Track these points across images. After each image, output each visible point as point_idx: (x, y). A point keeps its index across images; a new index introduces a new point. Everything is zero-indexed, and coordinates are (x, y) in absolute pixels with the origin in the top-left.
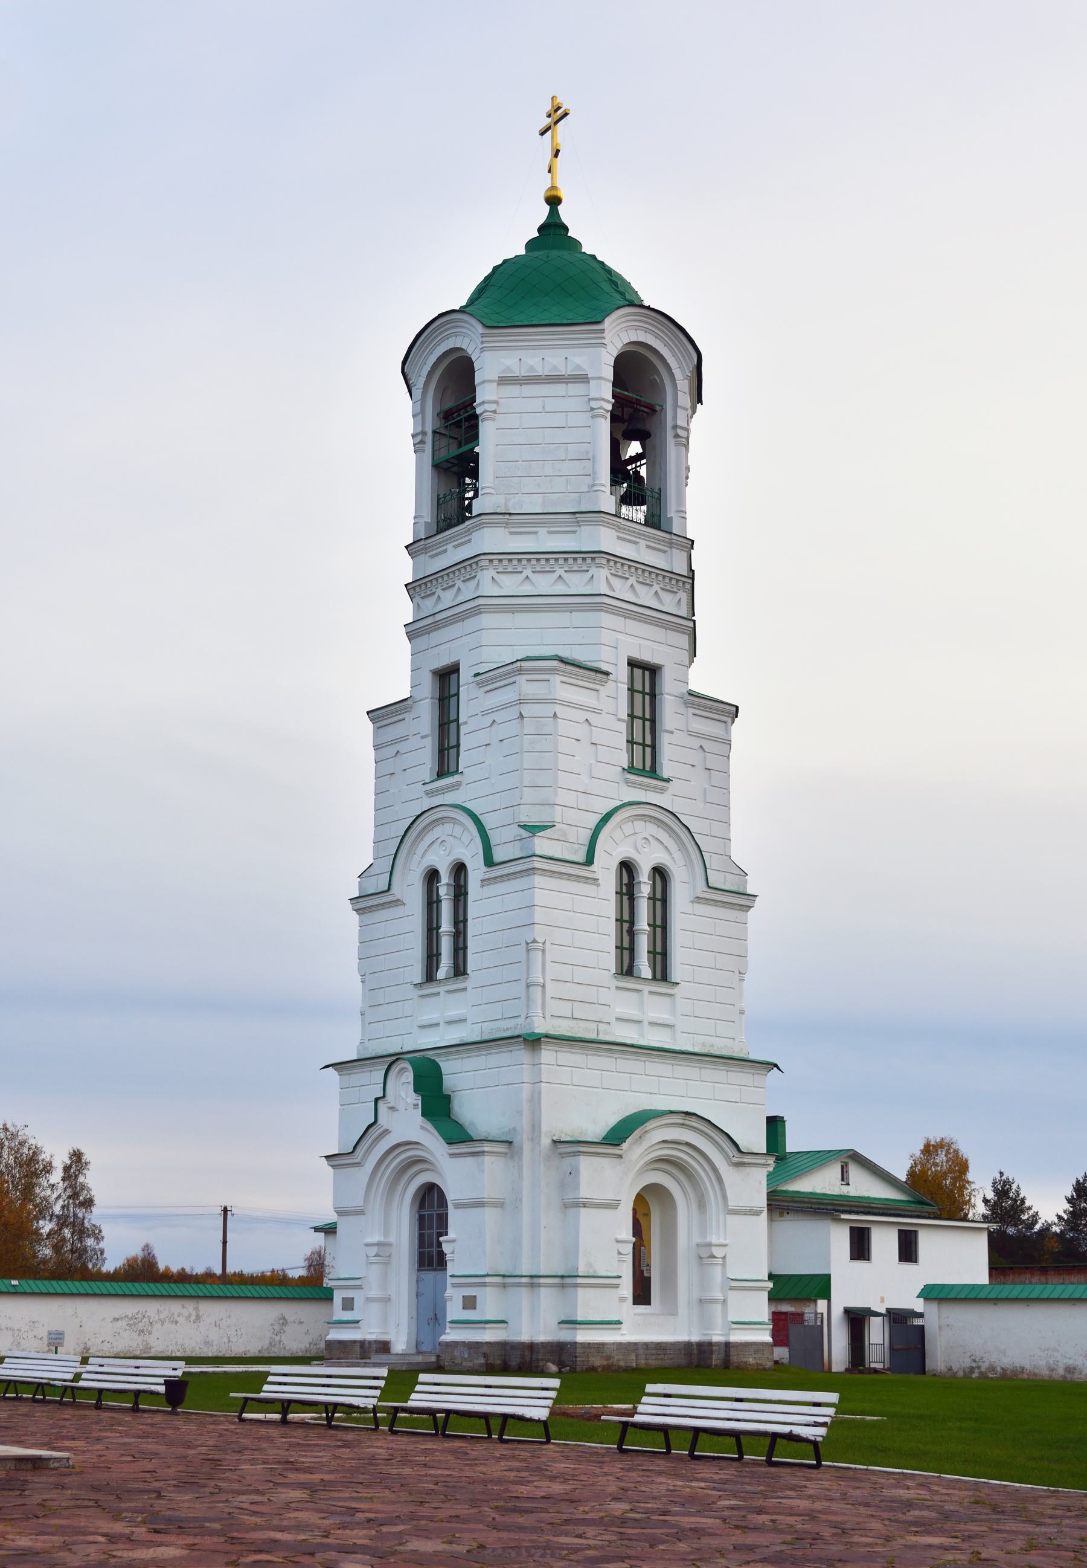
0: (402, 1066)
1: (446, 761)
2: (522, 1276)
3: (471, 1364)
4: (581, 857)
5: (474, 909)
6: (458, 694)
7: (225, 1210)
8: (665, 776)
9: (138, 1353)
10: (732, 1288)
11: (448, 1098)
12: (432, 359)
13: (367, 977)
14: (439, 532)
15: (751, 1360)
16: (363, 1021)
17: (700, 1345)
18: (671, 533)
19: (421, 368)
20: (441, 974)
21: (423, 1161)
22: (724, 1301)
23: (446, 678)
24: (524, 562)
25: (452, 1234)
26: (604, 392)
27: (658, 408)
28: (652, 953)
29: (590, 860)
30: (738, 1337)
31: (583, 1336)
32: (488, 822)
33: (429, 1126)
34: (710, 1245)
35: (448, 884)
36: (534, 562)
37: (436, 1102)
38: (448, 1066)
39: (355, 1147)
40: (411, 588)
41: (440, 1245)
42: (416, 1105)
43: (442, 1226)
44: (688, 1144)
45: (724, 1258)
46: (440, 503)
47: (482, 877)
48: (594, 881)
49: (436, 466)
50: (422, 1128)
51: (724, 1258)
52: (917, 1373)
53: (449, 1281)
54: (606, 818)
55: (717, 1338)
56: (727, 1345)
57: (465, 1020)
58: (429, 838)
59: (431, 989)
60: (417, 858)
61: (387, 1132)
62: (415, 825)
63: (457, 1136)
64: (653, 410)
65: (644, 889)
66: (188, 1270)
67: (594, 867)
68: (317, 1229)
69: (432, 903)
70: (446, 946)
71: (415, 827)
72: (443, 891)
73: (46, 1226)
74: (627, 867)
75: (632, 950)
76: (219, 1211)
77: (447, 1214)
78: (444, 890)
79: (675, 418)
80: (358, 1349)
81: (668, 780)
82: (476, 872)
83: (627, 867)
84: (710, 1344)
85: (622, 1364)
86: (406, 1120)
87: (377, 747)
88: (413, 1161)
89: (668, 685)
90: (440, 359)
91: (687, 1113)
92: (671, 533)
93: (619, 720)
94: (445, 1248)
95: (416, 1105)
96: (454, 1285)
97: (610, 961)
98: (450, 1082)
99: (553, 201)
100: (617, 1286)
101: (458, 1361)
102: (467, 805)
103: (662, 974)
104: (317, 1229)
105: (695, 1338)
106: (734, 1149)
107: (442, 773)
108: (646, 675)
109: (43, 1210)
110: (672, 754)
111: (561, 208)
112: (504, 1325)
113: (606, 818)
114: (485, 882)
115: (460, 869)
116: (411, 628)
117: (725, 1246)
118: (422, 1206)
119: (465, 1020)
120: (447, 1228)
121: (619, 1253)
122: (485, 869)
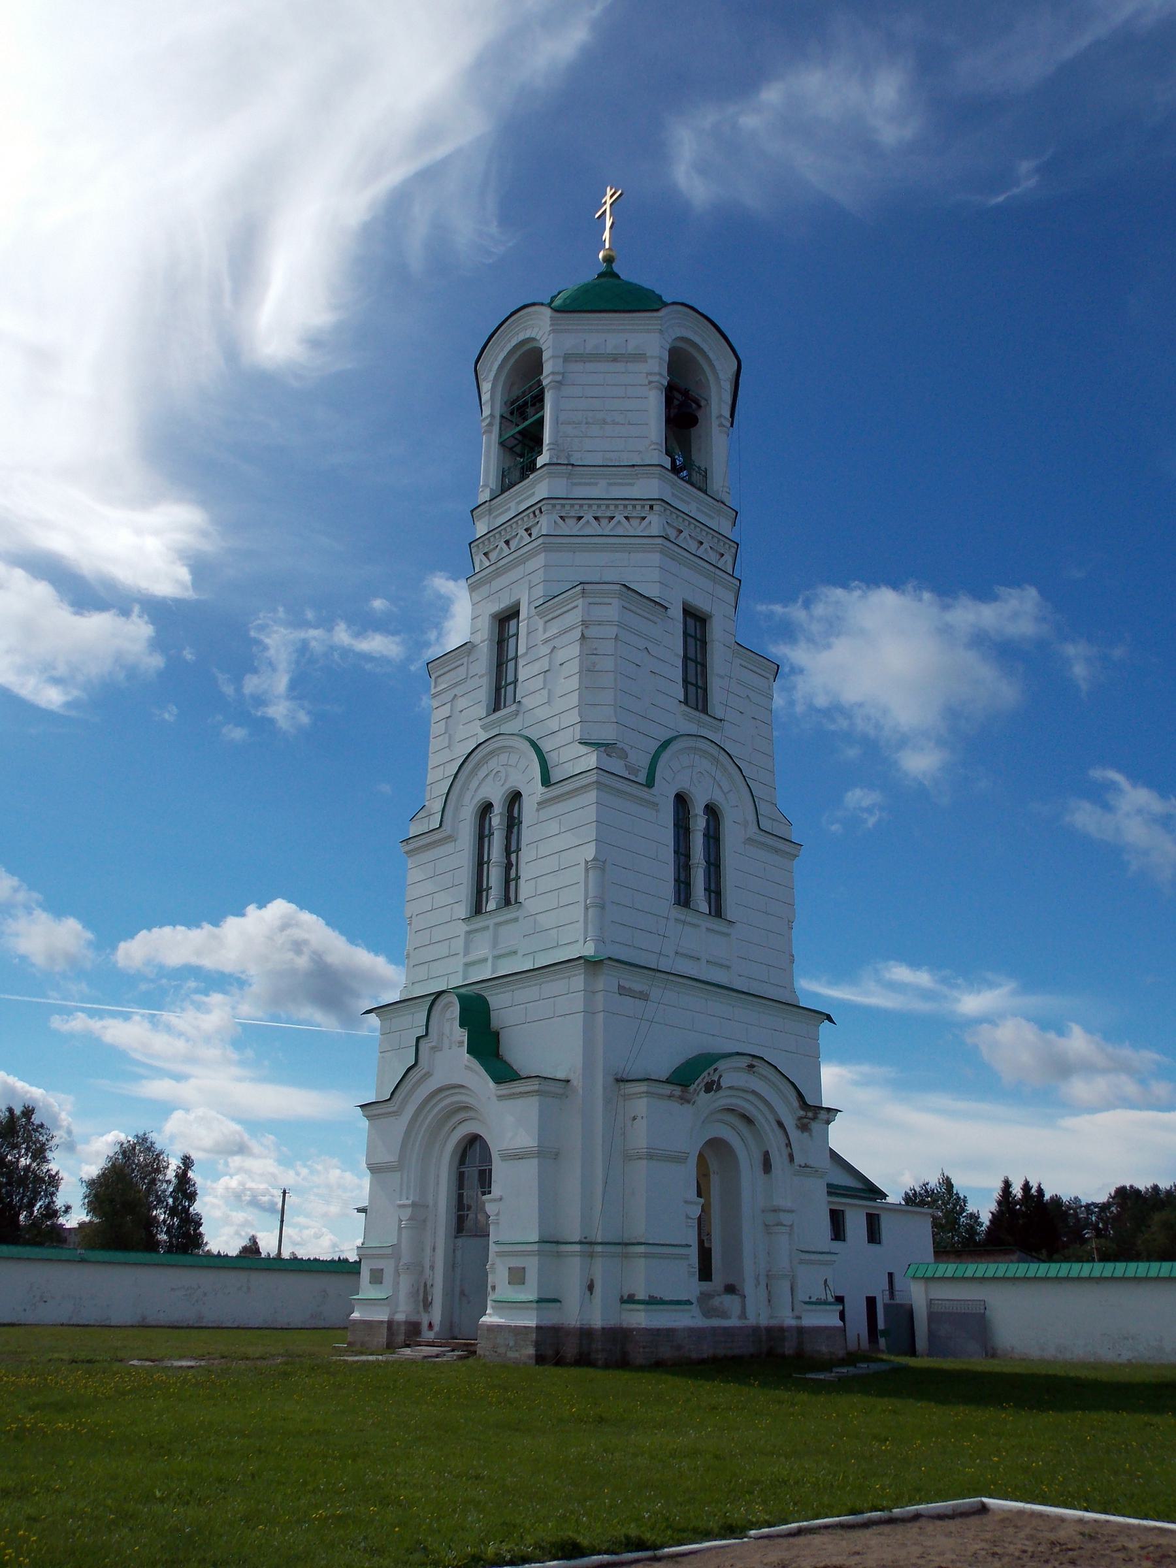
3: (516, 1355)
4: (642, 778)
8: (719, 715)
9: (191, 1323)
10: (802, 1262)
11: (497, 1035)
14: (503, 491)
15: (824, 1349)
17: (769, 1330)
19: (492, 364)
21: (467, 1108)
23: (506, 619)
24: (585, 508)
27: (703, 403)
28: (707, 889)
29: (650, 783)
31: (639, 1319)
34: (775, 1210)
37: (485, 1043)
38: (496, 1000)
39: (392, 1094)
43: (485, 1180)
44: (753, 1092)
47: (539, 800)
49: (502, 444)
50: (467, 1067)
51: (791, 1226)
52: (905, 1354)
53: (493, 1248)
54: (665, 745)
55: (790, 1322)
56: (801, 1330)
57: (515, 953)
59: (480, 922)
60: (469, 794)
61: (428, 1075)
63: (502, 1072)
65: (699, 823)
67: (654, 791)
69: (482, 836)
73: (160, 1214)
74: (681, 801)
75: (688, 884)
77: (490, 1170)
78: (497, 820)
82: (533, 792)
83: (681, 801)
84: (782, 1329)
85: (694, 1355)
86: (454, 1061)
89: (717, 632)
90: (511, 353)
91: (754, 1056)
93: (677, 655)
96: (500, 1254)
98: (497, 1020)
101: (502, 1350)
102: (525, 732)
103: (717, 910)
109: (160, 1201)
113: (665, 745)
114: (542, 804)
115: (515, 797)
118: (462, 1161)
119: (515, 953)
122: (543, 790)
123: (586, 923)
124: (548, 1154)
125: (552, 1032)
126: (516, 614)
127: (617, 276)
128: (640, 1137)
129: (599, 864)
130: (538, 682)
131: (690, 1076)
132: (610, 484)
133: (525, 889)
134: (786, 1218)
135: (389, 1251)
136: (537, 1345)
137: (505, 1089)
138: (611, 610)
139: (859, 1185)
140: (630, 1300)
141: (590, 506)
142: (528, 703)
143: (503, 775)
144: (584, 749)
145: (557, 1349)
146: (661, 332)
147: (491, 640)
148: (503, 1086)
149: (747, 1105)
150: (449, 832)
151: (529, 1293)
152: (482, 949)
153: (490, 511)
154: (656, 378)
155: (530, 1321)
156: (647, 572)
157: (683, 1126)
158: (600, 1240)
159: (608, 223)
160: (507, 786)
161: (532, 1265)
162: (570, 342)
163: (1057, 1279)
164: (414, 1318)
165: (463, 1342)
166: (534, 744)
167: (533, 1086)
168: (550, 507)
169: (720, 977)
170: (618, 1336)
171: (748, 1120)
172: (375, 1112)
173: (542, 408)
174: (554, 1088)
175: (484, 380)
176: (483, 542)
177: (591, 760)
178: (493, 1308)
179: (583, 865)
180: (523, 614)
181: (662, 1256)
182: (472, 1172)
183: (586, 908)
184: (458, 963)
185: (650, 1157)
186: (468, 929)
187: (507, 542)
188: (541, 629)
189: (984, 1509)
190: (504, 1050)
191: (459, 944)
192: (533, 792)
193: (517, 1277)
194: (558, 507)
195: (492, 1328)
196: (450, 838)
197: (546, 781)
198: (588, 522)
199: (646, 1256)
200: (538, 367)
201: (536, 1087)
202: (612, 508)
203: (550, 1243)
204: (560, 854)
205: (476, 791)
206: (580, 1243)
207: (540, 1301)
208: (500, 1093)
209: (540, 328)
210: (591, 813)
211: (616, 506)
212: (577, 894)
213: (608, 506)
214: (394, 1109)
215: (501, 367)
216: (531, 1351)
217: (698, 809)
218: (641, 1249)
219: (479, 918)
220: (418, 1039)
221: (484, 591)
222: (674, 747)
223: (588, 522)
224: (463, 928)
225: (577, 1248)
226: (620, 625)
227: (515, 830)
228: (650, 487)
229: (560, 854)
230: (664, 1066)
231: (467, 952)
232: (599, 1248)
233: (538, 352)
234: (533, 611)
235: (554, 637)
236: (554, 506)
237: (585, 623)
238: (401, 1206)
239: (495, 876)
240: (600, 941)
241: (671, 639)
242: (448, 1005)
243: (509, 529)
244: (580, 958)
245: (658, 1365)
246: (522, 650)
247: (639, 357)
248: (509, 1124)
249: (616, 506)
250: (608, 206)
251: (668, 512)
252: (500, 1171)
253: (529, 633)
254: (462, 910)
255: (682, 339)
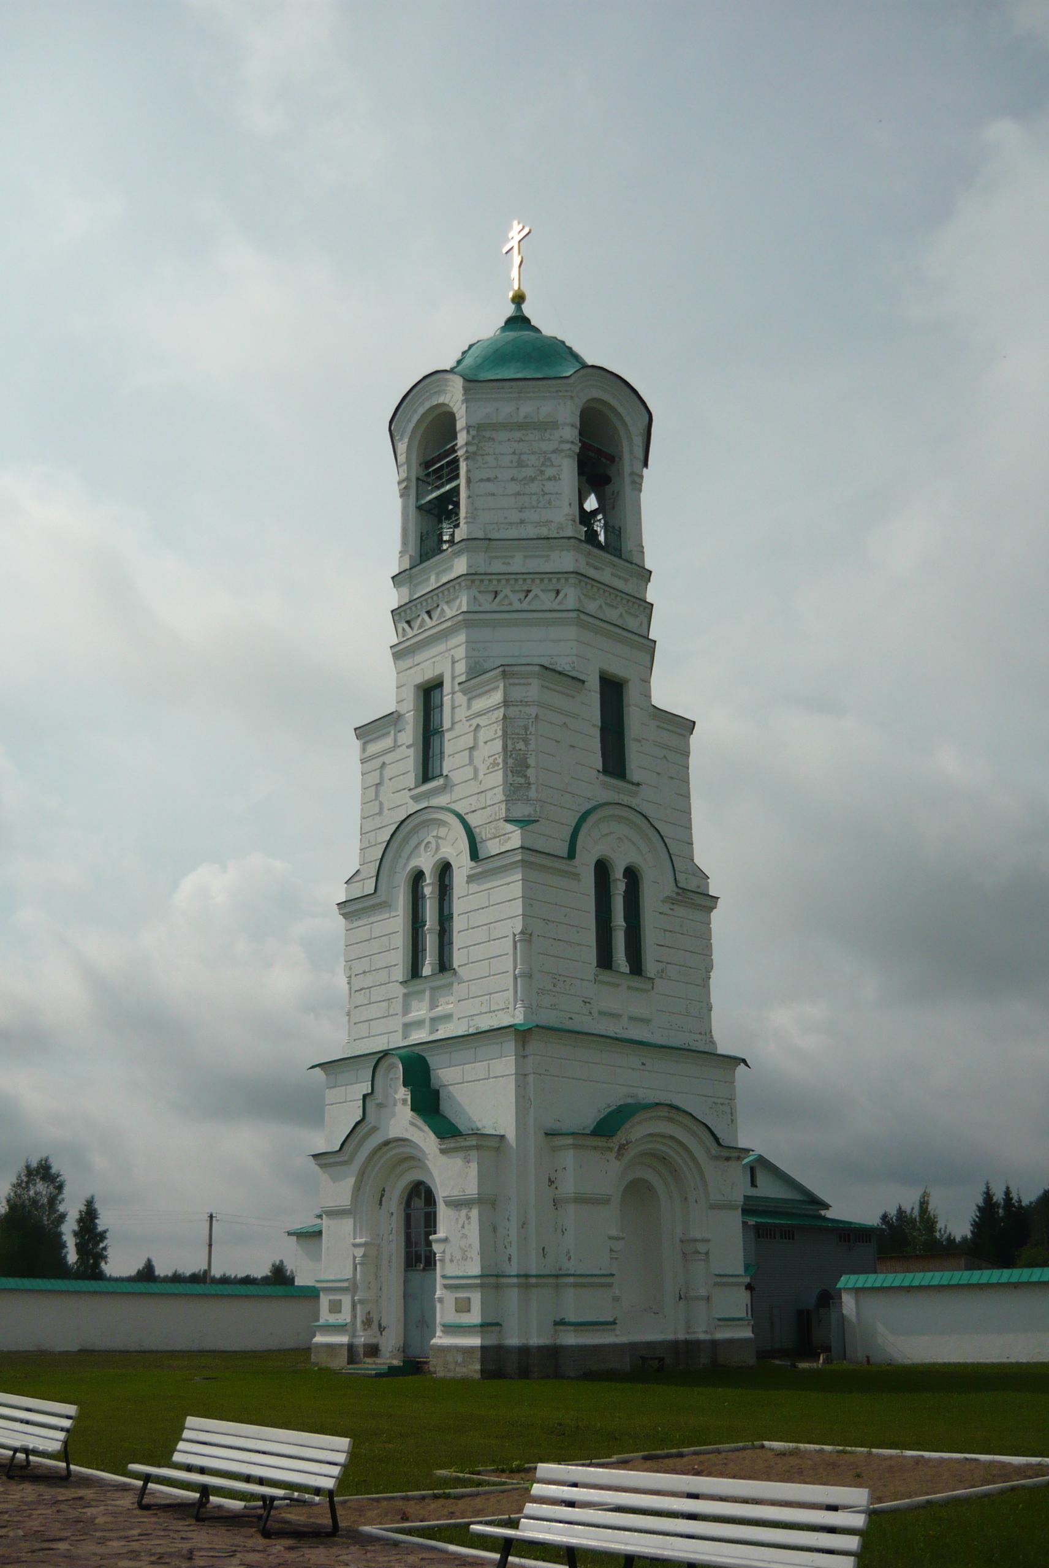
2: (509, 1276)
3: (464, 1370)
4: (564, 853)
5: (458, 906)
6: (442, 705)
7: (211, 1217)
8: (635, 779)
14: (421, 562)
18: (632, 563)
20: (427, 971)
21: (411, 1158)
22: (708, 1298)
23: (429, 693)
24: (503, 582)
25: (441, 1234)
29: (572, 855)
31: (570, 1339)
32: (474, 820)
33: (420, 1122)
35: (432, 884)
37: (428, 1102)
39: (342, 1145)
41: (429, 1244)
42: (404, 1101)
44: (672, 1138)
45: (707, 1254)
46: (422, 538)
48: (576, 876)
50: (412, 1124)
53: (439, 1281)
56: (714, 1343)
58: (413, 842)
60: (402, 861)
61: (375, 1129)
63: (447, 1131)
64: (613, 459)
65: (619, 888)
66: (180, 1271)
67: (576, 862)
71: (404, 833)
72: (427, 891)
74: (602, 869)
76: (206, 1217)
78: (429, 889)
79: (632, 465)
81: (638, 784)
84: (698, 1343)
86: (402, 1121)
88: (401, 1154)
92: (632, 563)
93: (594, 725)
94: (436, 1247)
95: (404, 1101)
97: (591, 954)
99: (519, 299)
100: (610, 1285)
102: (454, 806)
103: (636, 967)
108: (613, 691)
110: (636, 760)
111: (524, 306)
112: (498, 1328)
114: (471, 879)
115: (445, 870)
116: (396, 649)
120: (435, 1226)
121: (611, 1250)
122: (473, 864)
123: (516, 992)
124: (487, 1202)
125: (485, 1093)
126: (440, 685)
128: (568, 1186)
129: (527, 936)
130: (465, 757)
131: (608, 1127)
132: (525, 557)
133: (458, 958)
135: (346, 1284)
136: (483, 1361)
137: (451, 1144)
138: (533, 690)
140: (560, 1323)
142: (455, 777)
143: (434, 845)
144: (510, 827)
145: (500, 1364)
146: (572, 397)
148: (446, 1141)
149: (664, 1148)
150: (383, 899)
151: (475, 1317)
153: (411, 578)
154: (568, 446)
155: (476, 1341)
156: (564, 646)
157: (604, 1173)
158: (534, 1273)
159: (517, 260)
160: (437, 857)
161: (476, 1298)
162: (486, 410)
164: (373, 1341)
165: (413, 1366)
167: (473, 1142)
168: (469, 583)
169: (637, 1032)
170: (553, 1352)
171: (663, 1159)
172: (326, 1161)
173: (457, 477)
175: (401, 440)
177: (515, 838)
181: (583, 1285)
182: (419, 1218)
183: (515, 978)
184: (397, 1023)
186: (405, 991)
187: (429, 613)
188: (465, 704)
190: (445, 1107)
191: (397, 1006)
193: (463, 1306)
195: (442, 1349)
196: (386, 906)
197: (474, 855)
199: (575, 1285)
200: (452, 434)
201: (474, 1143)
202: (529, 581)
204: (490, 918)
206: (518, 1276)
209: (454, 396)
210: (517, 889)
211: (533, 580)
212: (507, 964)
214: (345, 1158)
215: (419, 422)
216: (478, 1367)
217: (618, 873)
218: (571, 1280)
220: (365, 1097)
221: (408, 662)
224: (402, 990)
226: (540, 704)
227: (447, 898)
228: (566, 560)
229: (490, 918)
230: (588, 1116)
231: (406, 1010)
232: (533, 1281)
234: (457, 688)
235: (479, 714)
236: (473, 581)
237: (506, 703)
238: (355, 1245)
240: (529, 1009)
241: (589, 706)
242: (392, 1066)
244: (510, 1026)
245: (591, 1376)
246: (447, 724)
248: (451, 1175)
249: (533, 580)
250: (514, 243)
251: (583, 584)
252: (444, 1216)
254: (400, 972)
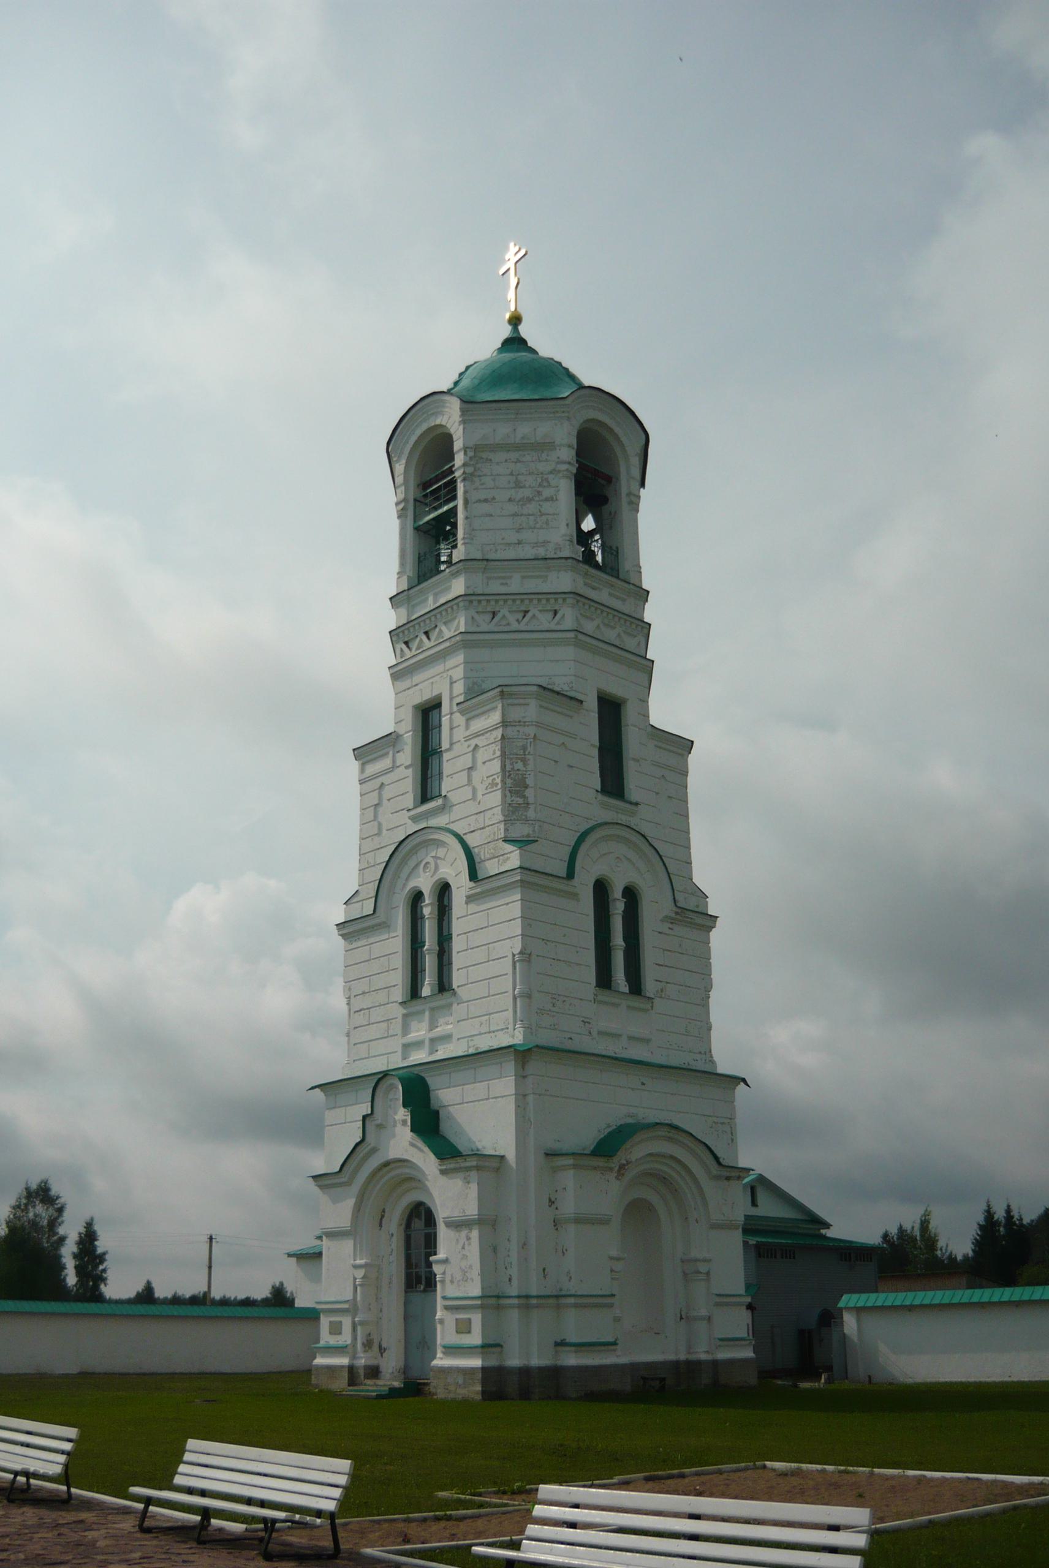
0: (392, 1081)
1: (427, 788)
4: (561, 870)
6: (440, 726)
7: (211, 1238)
8: (633, 799)
12: (414, 439)
13: (353, 1000)
14: (419, 583)
16: (349, 1043)
17: (688, 1363)
18: (629, 583)
20: (426, 991)
21: (410, 1179)
23: (428, 715)
25: (441, 1255)
26: (567, 454)
29: (570, 875)
30: (723, 1355)
31: (571, 1360)
32: (472, 841)
33: (420, 1143)
36: (510, 602)
37: (428, 1122)
40: (394, 634)
41: (429, 1265)
42: (404, 1122)
43: (431, 1243)
44: (672, 1157)
45: (708, 1273)
46: (420, 559)
48: (574, 896)
50: (412, 1145)
56: (715, 1363)
58: (412, 863)
59: (417, 1006)
61: (374, 1150)
62: (400, 849)
63: (447, 1151)
65: (618, 907)
67: (576, 881)
68: (290, 1255)
70: (430, 963)
71: (404, 853)
72: (427, 911)
74: (601, 888)
76: (206, 1239)
78: (428, 910)
80: (346, 1375)
81: (637, 804)
82: (461, 886)
84: (699, 1363)
86: (401, 1141)
87: (362, 782)
94: (436, 1268)
95: (404, 1122)
97: (591, 975)
100: (611, 1306)
104: (290, 1255)
105: (683, 1357)
106: (714, 1162)
107: (425, 796)
108: (610, 712)
112: (499, 1349)
114: (470, 899)
115: (444, 890)
116: (393, 671)
117: (709, 1261)
120: (435, 1247)
121: (612, 1271)
122: (472, 884)
124: (487, 1222)
125: (485, 1113)
127: (523, 342)
128: (568, 1206)
129: (526, 956)
131: (608, 1147)
132: (523, 577)
134: (703, 1268)
135: (346, 1306)
136: (484, 1382)
137: (451, 1164)
139: (799, 1217)
140: (561, 1344)
141: (505, 601)
142: (454, 797)
143: (432, 866)
144: (509, 847)
145: (498, 1384)
146: (569, 419)
147: (414, 730)
149: (665, 1168)
151: (475, 1338)
152: (420, 1031)
155: (476, 1362)
156: (561, 666)
157: (605, 1194)
159: (513, 281)
160: (436, 878)
161: (476, 1319)
163: (1018, 1304)
165: (414, 1388)
166: (457, 836)
168: (467, 603)
170: (554, 1373)
171: (664, 1179)
174: (489, 1166)
175: (398, 461)
176: (403, 632)
178: (444, 1353)
179: (510, 956)
180: (445, 708)
182: (419, 1238)
183: (515, 998)
184: (396, 1044)
185: (579, 1220)
186: (405, 1011)
189: (765, 1467)
191: (397, 1026)
192: (461, 886)
194: (475, 603)
197: (473, 875)
198: (504, 616)
199: (576, 1306)
201: (474, 1163)
202: (527, 602)
203: (492, 1302)
204: (489, 938)
205: (407, 879)
206: (519, 1297)
207: (483, 1347)
208: (444, 1167)
209: (451, 418)
210: (516, 910)
212: (507, 983)
213: (522, 600)
216: (479, 1388)
217: (617, 893)
218: (572, 1300)
219: (414, 1002)
220: (364, 1118)
222: (590, 839)
223: (504, 616)
225: (515, 1301)
226: (539, 725)
228: (564, 580)
229: (489, 938)
230: (587, 1137)
232: (534, 1301)
233: (448, 439)
234: (455, 708)
235: (477, 735)
237: (505, 723)
238: (355, 1267)
239: (430, 963)
240: (529, 1030)
242: (392, 1087)
243: (428, 621)
244: (510, 1047)
245: (592, 1397)
246: (445, 745)
247: (544, 447)
248: (451, 1196)
249: (531, 600)
250: (511, 264)
251: (580, 604)
252: (444, 1236)
253: (451, 729)
254: (399, 993)
255: (588, 421)
